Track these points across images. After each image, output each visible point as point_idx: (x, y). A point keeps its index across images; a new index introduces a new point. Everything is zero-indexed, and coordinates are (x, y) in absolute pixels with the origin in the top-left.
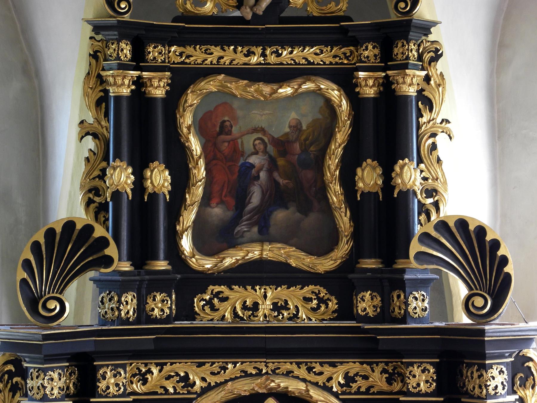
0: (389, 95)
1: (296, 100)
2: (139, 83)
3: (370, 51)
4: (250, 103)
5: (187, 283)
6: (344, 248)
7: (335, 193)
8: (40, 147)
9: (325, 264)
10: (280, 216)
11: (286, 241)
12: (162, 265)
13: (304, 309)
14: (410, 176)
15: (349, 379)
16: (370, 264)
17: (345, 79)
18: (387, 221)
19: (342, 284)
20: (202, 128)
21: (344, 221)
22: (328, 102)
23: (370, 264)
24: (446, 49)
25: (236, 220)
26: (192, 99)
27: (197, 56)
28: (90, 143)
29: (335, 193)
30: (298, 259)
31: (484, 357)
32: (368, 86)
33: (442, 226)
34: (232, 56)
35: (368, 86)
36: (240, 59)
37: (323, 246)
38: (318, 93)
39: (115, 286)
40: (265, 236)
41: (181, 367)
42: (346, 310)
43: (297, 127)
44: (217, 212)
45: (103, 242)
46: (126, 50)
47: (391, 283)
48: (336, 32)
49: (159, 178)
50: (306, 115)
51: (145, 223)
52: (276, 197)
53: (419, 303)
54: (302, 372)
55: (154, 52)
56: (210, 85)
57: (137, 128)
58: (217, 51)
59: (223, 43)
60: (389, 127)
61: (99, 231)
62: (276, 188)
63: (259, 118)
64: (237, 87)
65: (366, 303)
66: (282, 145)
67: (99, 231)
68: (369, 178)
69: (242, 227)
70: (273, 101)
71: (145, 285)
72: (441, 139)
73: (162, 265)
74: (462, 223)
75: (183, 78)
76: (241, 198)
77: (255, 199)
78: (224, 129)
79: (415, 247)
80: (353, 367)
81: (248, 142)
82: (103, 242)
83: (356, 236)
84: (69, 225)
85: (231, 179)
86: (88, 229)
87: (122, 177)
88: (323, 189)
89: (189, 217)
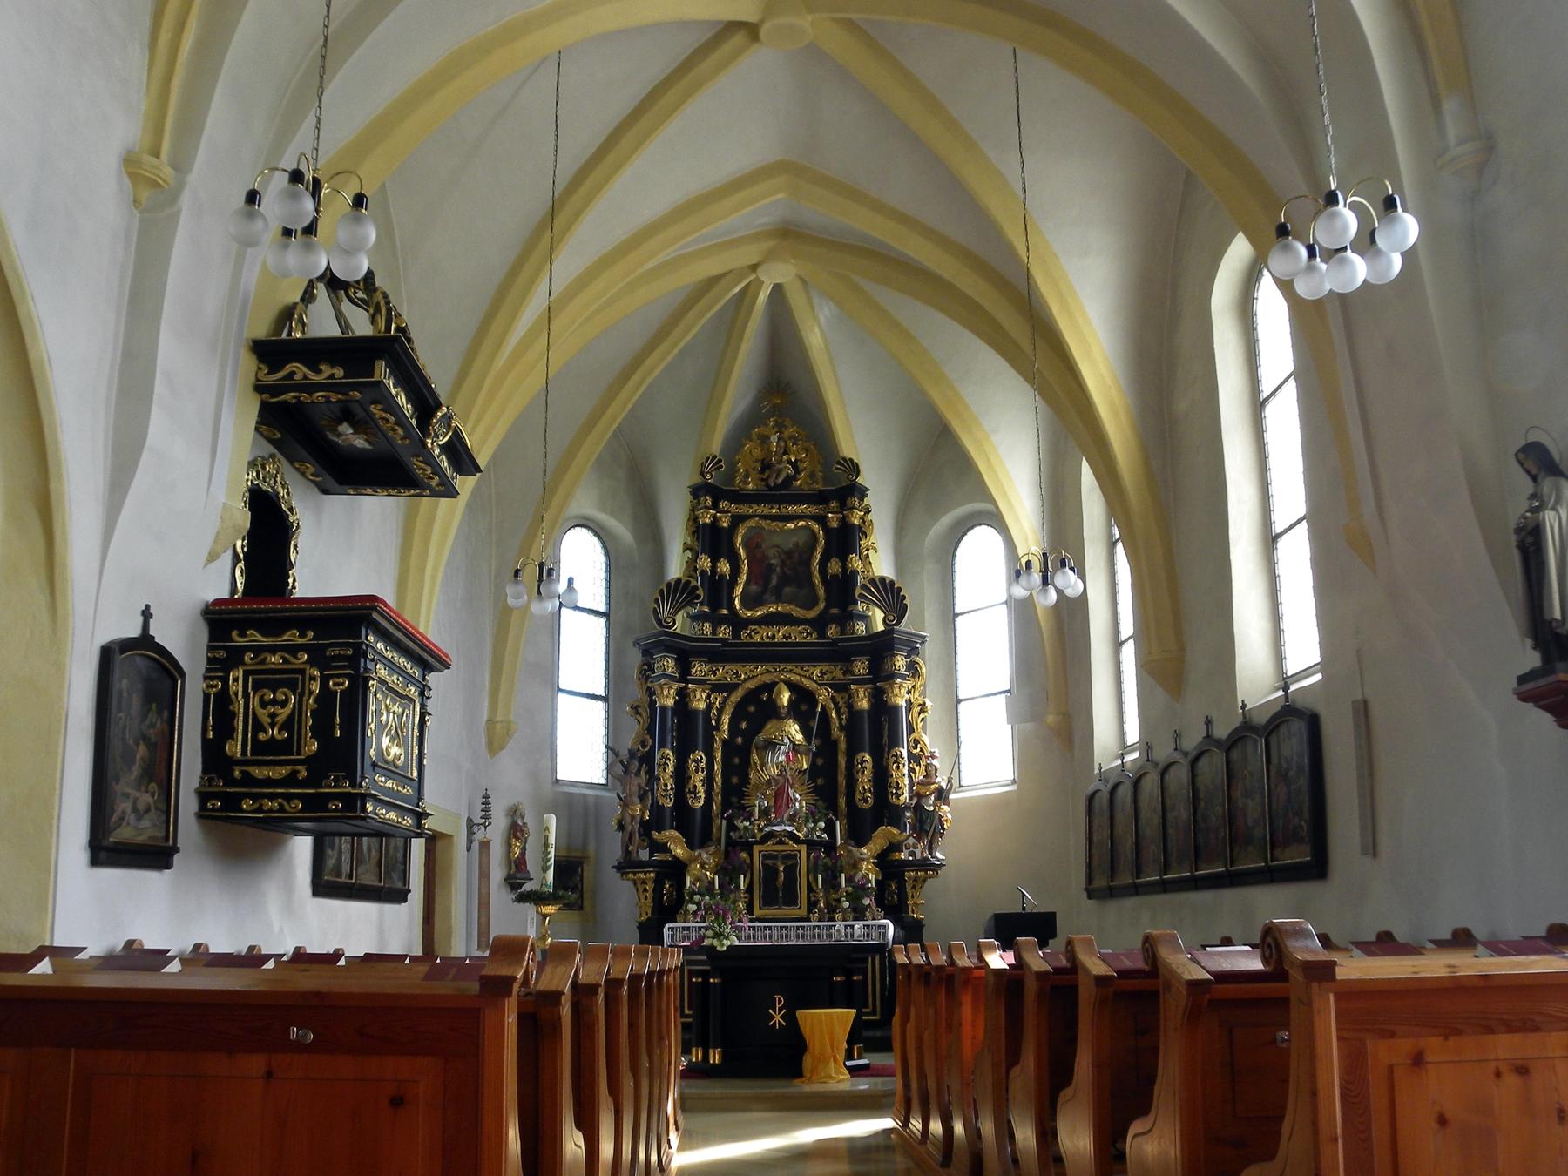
0: (844, 522)
1: (797, 526)
2: (715, 517)
3: (861, 667)
4: (773, 532)
5: (739, 624)
6: (822, 605)
7: (817, 580)
8: (689, 239)
9: (812, 614)
10: (787, 590)
11: (790, 603)
12: (725, 612)
13: (798, 634)
14: (856, 563)
15: (823, 674)
16: (835, 611)
17: (822, 520)
18: (843, 590)
19: (819, 624)
20: (745, 544)
21: (821, 590)
22: (813, 531)
23: (835, 611)
24: (873, 508)
25: (763, 592)
26: (742, 530)
27: (744, 509)
28: (688, 553)
29: (817, 580)
30: (797, 612)
31: (893, 649)
32: (834, 521)
33: (873, 581)
34: (762, 509)
35: (834, 521)
36: (767, 511)
37: (811, 603)
38: (807, 527)
39: (698, 618)
40: (778, 600)
41: (733, 667)
42: (822, 635)
43: (796, 545)
44: (754, 588)
45: (696, 588)
46: (709, 502)
47: (847, 617)
48: (821, 498)
49: (724, 567)
50: (801, 539)
51: (718, 589)
52: (785, 580)
53: (860, 628)
54: (798, 670)
55: (723, 504)
56: (751, 523)
57: (711, 540)
58: (755, 507)
59: (758, 502)
60: (846, 539)
61: (693, 583)
62: (783, 576)
63: (776, 540)
64: (763, 523)
65: (832, 631)
66: (789, 554)
67: (693, 583)
68: (834, 567)
69: (767, 596)
70: (783, 531)
71: (717, 622)
72: (871, 552)
73: (725, 612)
74: (882, 579)
75: (737, 520)
76: (767, 581)
77: (774, 581)
78: (758, 546)
79: (858, 591)
80: (825, 667)
81: (771, 552)
82: (696, 588)
83: (827, 599)
84: (678, 581)
85: (761, 572)
86: (688, 583)
87: (705, 563)
88: (810, 575)
89: (739, 590)
